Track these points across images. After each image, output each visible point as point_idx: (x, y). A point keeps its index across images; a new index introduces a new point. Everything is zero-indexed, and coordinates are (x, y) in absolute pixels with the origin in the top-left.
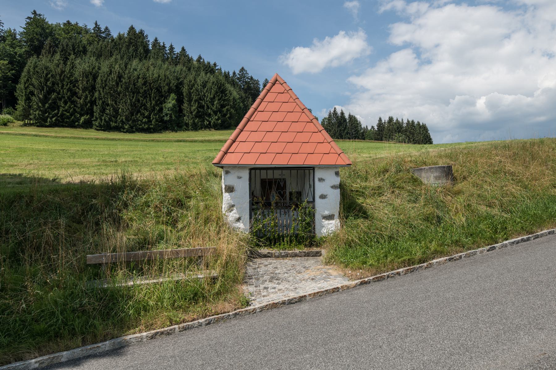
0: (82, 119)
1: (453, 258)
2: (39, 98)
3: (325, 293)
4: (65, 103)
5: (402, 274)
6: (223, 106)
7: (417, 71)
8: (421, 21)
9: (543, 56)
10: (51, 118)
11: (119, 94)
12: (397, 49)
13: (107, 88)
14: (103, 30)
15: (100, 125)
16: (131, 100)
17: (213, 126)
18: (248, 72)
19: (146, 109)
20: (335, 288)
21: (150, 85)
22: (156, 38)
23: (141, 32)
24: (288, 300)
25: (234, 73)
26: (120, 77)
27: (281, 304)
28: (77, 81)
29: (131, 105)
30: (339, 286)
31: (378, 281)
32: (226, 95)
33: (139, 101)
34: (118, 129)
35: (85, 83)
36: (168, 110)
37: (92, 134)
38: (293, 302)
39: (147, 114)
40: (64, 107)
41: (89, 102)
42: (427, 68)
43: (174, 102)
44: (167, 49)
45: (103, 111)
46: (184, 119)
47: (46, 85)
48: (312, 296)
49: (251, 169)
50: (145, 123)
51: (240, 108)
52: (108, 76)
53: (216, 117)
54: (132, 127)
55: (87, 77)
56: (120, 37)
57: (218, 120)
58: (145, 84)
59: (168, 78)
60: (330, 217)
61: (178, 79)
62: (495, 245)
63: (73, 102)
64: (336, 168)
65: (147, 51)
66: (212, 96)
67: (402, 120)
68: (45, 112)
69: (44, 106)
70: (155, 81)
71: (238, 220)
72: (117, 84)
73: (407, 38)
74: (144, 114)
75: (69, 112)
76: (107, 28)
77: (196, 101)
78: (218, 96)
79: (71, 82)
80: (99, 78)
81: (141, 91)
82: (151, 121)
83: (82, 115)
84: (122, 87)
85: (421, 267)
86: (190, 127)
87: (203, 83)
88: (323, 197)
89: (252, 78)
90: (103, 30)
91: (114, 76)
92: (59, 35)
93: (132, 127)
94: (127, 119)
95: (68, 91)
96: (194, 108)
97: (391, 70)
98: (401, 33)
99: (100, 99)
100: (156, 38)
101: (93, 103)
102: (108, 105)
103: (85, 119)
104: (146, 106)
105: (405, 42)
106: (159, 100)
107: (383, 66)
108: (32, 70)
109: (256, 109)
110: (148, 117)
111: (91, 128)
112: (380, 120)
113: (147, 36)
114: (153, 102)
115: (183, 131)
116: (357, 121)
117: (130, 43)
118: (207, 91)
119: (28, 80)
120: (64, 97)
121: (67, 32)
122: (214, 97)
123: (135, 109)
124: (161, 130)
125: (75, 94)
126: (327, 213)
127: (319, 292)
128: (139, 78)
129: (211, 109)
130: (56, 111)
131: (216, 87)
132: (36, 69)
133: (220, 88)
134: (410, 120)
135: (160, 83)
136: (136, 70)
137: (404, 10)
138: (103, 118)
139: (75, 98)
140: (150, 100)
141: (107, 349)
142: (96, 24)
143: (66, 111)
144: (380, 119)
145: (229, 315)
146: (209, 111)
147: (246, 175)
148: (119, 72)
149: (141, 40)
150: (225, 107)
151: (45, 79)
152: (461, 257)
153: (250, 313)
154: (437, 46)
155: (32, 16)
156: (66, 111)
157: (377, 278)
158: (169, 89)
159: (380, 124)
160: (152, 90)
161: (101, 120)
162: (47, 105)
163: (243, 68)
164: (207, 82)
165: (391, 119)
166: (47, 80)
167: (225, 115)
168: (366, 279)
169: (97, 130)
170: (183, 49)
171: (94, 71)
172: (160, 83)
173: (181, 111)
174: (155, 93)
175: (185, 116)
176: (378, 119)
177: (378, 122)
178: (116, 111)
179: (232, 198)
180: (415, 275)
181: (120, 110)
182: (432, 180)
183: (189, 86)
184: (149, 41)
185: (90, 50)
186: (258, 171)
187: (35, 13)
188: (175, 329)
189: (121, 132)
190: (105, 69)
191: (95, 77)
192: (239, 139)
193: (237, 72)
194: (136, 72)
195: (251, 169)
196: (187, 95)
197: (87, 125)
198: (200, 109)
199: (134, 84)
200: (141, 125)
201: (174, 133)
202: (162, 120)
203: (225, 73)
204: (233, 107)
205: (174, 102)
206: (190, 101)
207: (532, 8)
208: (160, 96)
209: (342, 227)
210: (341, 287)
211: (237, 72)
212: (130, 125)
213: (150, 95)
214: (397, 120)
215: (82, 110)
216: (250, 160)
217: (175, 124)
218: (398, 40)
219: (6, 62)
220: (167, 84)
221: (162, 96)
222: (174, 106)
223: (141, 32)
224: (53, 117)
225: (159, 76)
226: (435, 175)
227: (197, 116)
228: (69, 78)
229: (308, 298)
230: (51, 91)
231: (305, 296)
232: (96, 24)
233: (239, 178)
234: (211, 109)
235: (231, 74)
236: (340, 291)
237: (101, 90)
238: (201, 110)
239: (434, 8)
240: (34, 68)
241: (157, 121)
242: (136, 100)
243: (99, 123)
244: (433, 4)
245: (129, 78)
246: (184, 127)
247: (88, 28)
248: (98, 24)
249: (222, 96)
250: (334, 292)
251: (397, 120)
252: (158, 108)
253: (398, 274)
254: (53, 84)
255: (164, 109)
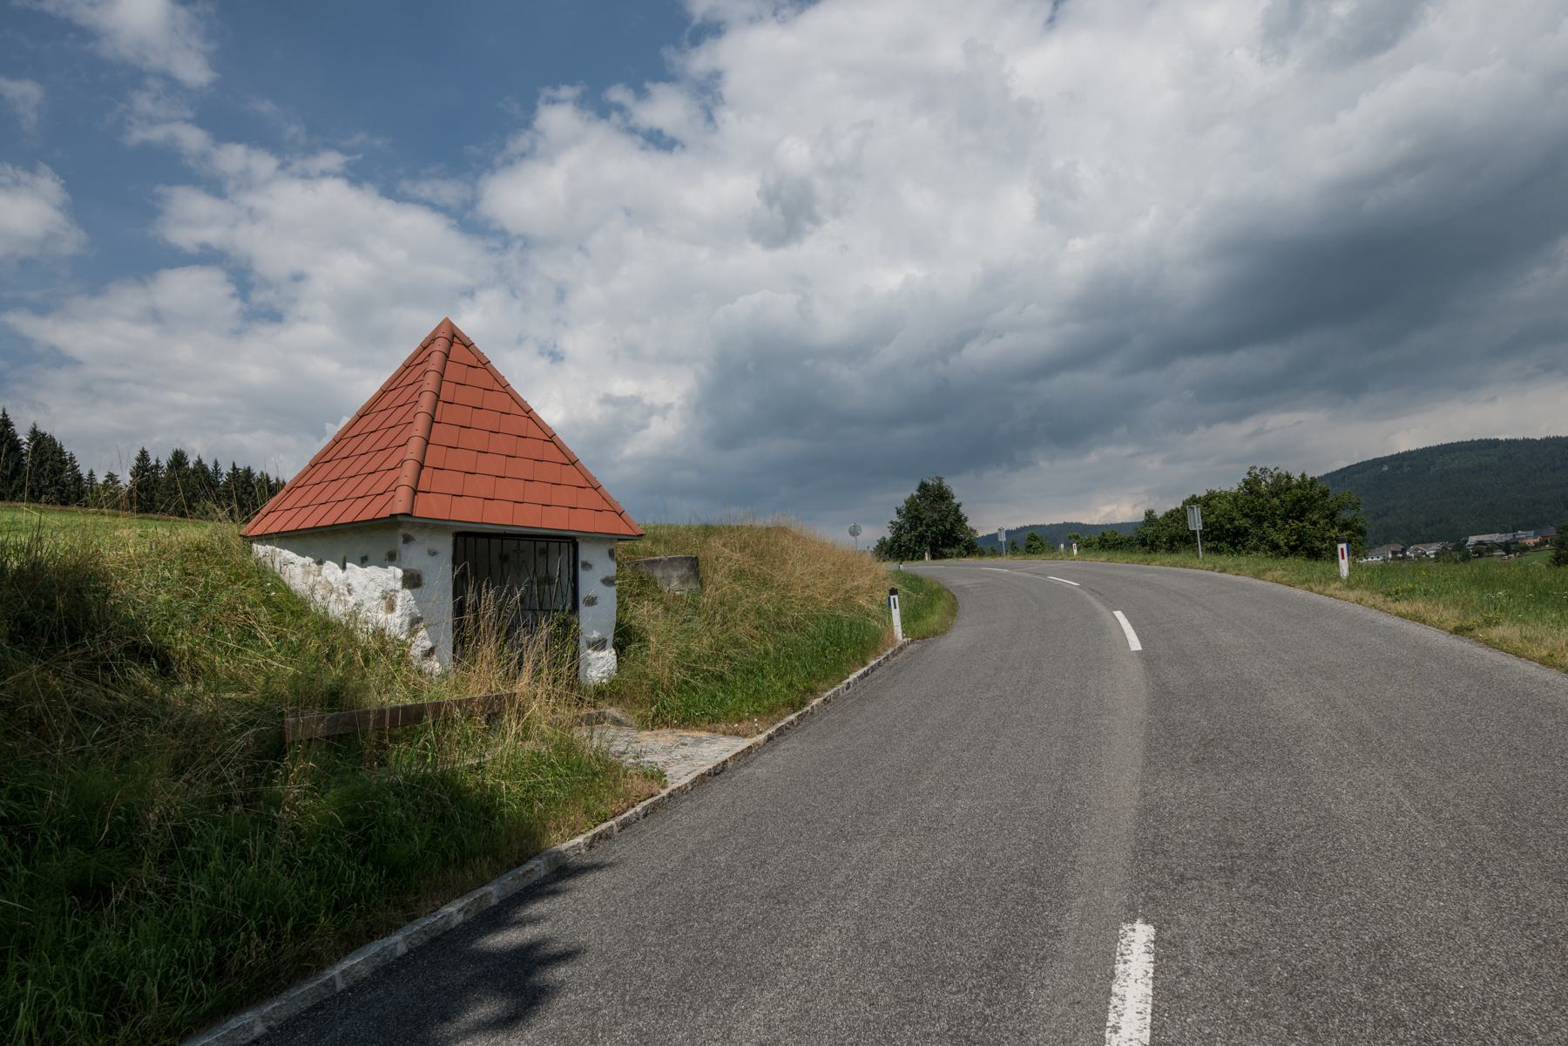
7: (237, 333)
8: (255, 200)
9: (541, 354)
12: (180, 259)
30: (726, 756)
42: (266, 330)
49: (457, 535)
60: (599, 645)
64: (611, 540)
67: (216, 464)
71: (429, 653)
73: (212, 235)
97: (155, 316)
98: (193, 217)
105: (205, 246)
107: (129, 298)
112: (144, 456)
116: (61, 452)
126: (596, 635)
134: (241, 466)
137: (204, 157)
141: (543, 873)
144: (143, 453)
147: (445, 546)
154: (298, 278)
159: (143, 466)
165: (179, 459)
176: (137, 454)
177: (135, 463)
179: (418, 602)
182: (675, 584)
186: (471, 540)
195: (457, 535)
207: (518, 244)
214: (200, 462)
216: (469, 513)
218: (184, 237)
233: (433, 553)
239: (293, 175)
244: (289, 164)
251: (200, 462)
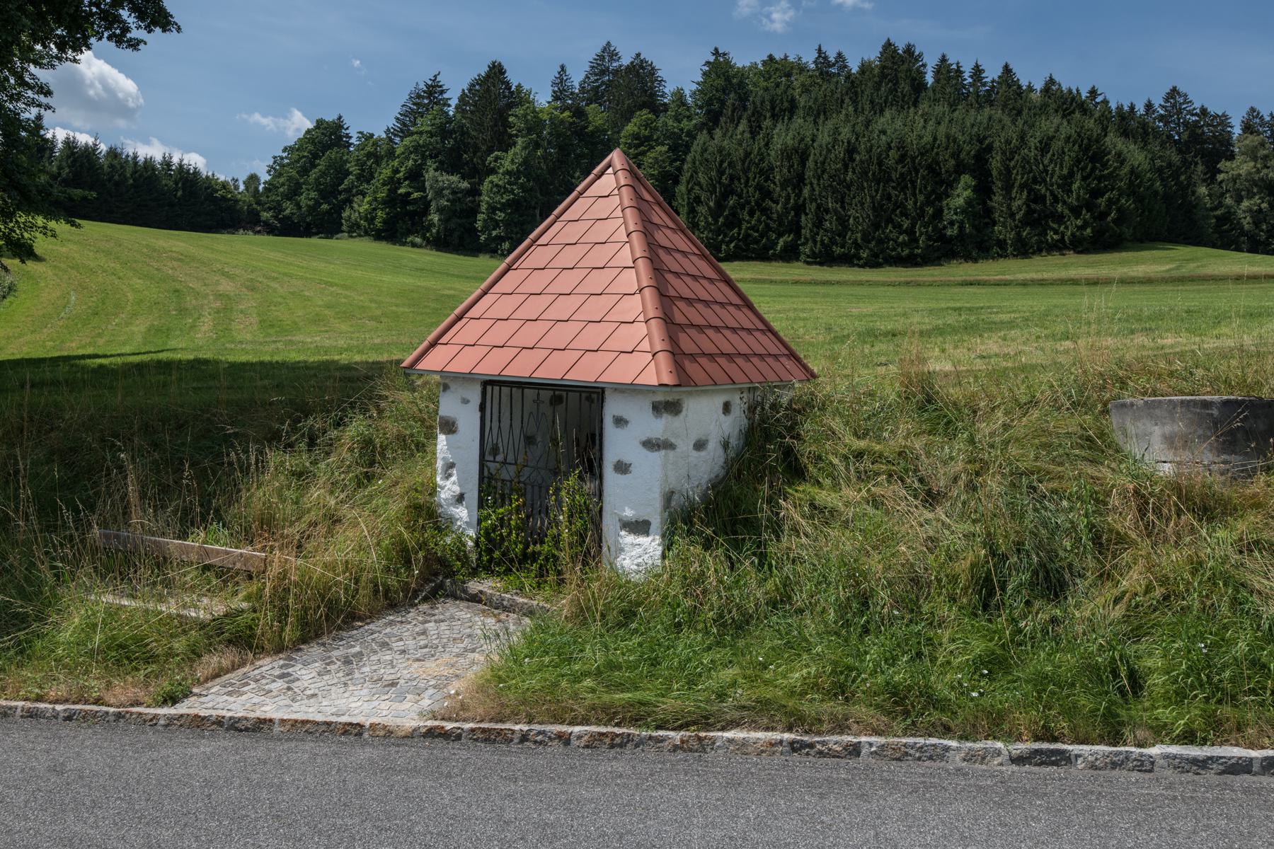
0: (781, 242)
1: (811, 746)
2: (709, 208)
3: (324, 728)
4: (751, 214)
5: (575, 742)
6: (1096, 193)
10: (728, 244)
11: (848, 187)
13: (826, 176)
14: (832, 59)
15: (814, 253)
16: (872, 197)
17: (1072, 242)
18: (1190, 98)
19: (905, 214)
20: (351, 724)
21: (913, 162)
22: (944, 56)
23: (909, 50)
24: (231, 718)
25: (1149, 106)
26: (851, 150)
27: (214, 723)
28: (772, 169)
29: (874, 209)
31: (486, 740)
32: (1105, 166)
33: (889, 198)
34: (847, 260)
35: (785, 170)
36: (956, 214)
37: (797, 271)
38: (239, 725)
39: (906, 224)
40: (748, 222)
41: (792, 209)
43: (968, 193)
44: (966, 75)
45: (819, 223)
46: (993, 232)
47: (720, 183)
48: (288, 727)
50: (904, 244)
51: (1156, 192)
52: (829, 151)
53: (1079, 222)
54: (876, 256)
55: (789, 158)
56: (865, 68)
57: (1083, 228)
58: (902, 159)
59: (955, 141)
60: (639, 527)
61: (981, 141)
62: (1075, 749)
63: (765, 211)
65: (918, 85)
66: (1065, 172)
68: (718, 232)
69: (716, 221)
70: (923, 152)
71: (460, 499)
72: (846, 166)
74: (900, 226)
75: (757, 231)
76: (840, 55)
77: (1022, 187)
78: (1083, 169)
79: (761, 172)
80: (811, 158)
81: (894, 176)
82: (917, 241)
83: (780, 235)
84: (854, 172)
85: (660, 740)
86: (1010, 250)
87: (1040, 142)
88: (622, 468)
89: (1204, 111)
90: (832, 59)
91: (840, 151)
92: (755, 85)
93: (876, 256)
94: (866, 239)
95: (756, 188)
96: (1016, 204)
99: (813, 200)
100: (944, 56)
101: (800, 209)
102: (827, 211)
103: (786, 242)
104: (905, 207)
106: (933, 191)
108: (698, 157)
109: (534, 241)
110: (910, 232)
111: (797, 259)
113: (920, 55)
114: (921, 198)
115: (993, 258)
117: (883, 76)
118: (1051, 161)
119: (692, 176)
120: (749, 203)
121: (766, 75)
122: (1071, 174)
123: (882, 215)
124: (939, 258)
125: (767, 194)
126: (629, 513)
127: (308, 722)
128: (890, 148)
129: (1064, 203)
130: (736, 230)
131: (1076, 147)
132: (705, 155)
133: (1087, 149)
135: (937, 154)
136: (884, 132)
138: (819, 238)
139: (768, 203)
140: (914, 195)
142: (820, 50)
143: (752, 228)
145: (107, 713)
146: (1060, 207)
147: (475, 395)
148: (849, 142)
149: (905, 67)
150: (1102, 195)
151: (718, 171)
152: (855, 750)
153: (145, 721)
155: (712, 59)
156: (752, 228)
157: (484, 731)
158: (957, 165)
160: (917, 172)
161: (815, 242)
162: (721, 220)
163: (1174, 90)
164: (1051, 138)
166: (721, 173)
167: (1103, 215)
168: (449, 726)
169: (808, 263)
170: (1007, 70)
171: (802, 146)
172: (937, 154)
173: (989, 212)
174: (923, 178)
175: (994, 223)
178: (843, 221)
180: (619, 764)
181: (851, 221)
183: (1004, 153)
184: (924, 66)
185: (802, 104)
187: (716, 52)
188: (16, 708)
189: (854, 265)
190: (824, 138)
191: (803, 161)
192: (468, 315)
193: (1158, 101)
194: (883, 138)
196: (1000, 173)
197: (790, 255)
198: (1033, 206)
199: (880, 164)
200: (894, 249)
201: (970, 264)
202: (942, 238)
203: (1120, 108)
204: (1132, 191)
205: (968, 193)
206: (1008, 188)
208: (936, 183)
209: (664, 557)
210: (371, 725)
211: (1158, 101)
212: (871, 250)
213: (913, 182)
215: (780, 225)
217: (975, 242)
219: (665, 148)
220: (952, 156)
221: (942, 182)
222: (969, 202)
223: (909, 50)
224: (731, 242)
225: (935, 139)
226: (1168, 429)
227: (1026, 222)
228: (757, 165)
229: (277, 729)
230: (728, 192)
231: (271, 720)
232: (820, 50)
234: (1064, 203)
235: (1140, 109)
236: (366, 735)
237: (815, 182)
238: (1038, 207)
240: (702, 155)
241: (929, 238)
242: (883, 195)
243: (811, 250)
245: (869, 151)
246: (996, 249)
247: (804, 60)
248: (823, 49)
249: (1093, 170)
250: (345, 733)
252: (930, 210)
253: (565, 739)
254: (732, 178)
255: (946, 211)
